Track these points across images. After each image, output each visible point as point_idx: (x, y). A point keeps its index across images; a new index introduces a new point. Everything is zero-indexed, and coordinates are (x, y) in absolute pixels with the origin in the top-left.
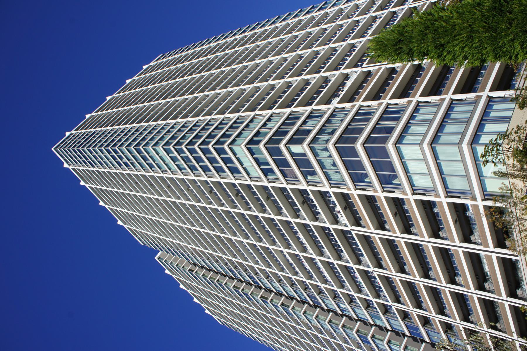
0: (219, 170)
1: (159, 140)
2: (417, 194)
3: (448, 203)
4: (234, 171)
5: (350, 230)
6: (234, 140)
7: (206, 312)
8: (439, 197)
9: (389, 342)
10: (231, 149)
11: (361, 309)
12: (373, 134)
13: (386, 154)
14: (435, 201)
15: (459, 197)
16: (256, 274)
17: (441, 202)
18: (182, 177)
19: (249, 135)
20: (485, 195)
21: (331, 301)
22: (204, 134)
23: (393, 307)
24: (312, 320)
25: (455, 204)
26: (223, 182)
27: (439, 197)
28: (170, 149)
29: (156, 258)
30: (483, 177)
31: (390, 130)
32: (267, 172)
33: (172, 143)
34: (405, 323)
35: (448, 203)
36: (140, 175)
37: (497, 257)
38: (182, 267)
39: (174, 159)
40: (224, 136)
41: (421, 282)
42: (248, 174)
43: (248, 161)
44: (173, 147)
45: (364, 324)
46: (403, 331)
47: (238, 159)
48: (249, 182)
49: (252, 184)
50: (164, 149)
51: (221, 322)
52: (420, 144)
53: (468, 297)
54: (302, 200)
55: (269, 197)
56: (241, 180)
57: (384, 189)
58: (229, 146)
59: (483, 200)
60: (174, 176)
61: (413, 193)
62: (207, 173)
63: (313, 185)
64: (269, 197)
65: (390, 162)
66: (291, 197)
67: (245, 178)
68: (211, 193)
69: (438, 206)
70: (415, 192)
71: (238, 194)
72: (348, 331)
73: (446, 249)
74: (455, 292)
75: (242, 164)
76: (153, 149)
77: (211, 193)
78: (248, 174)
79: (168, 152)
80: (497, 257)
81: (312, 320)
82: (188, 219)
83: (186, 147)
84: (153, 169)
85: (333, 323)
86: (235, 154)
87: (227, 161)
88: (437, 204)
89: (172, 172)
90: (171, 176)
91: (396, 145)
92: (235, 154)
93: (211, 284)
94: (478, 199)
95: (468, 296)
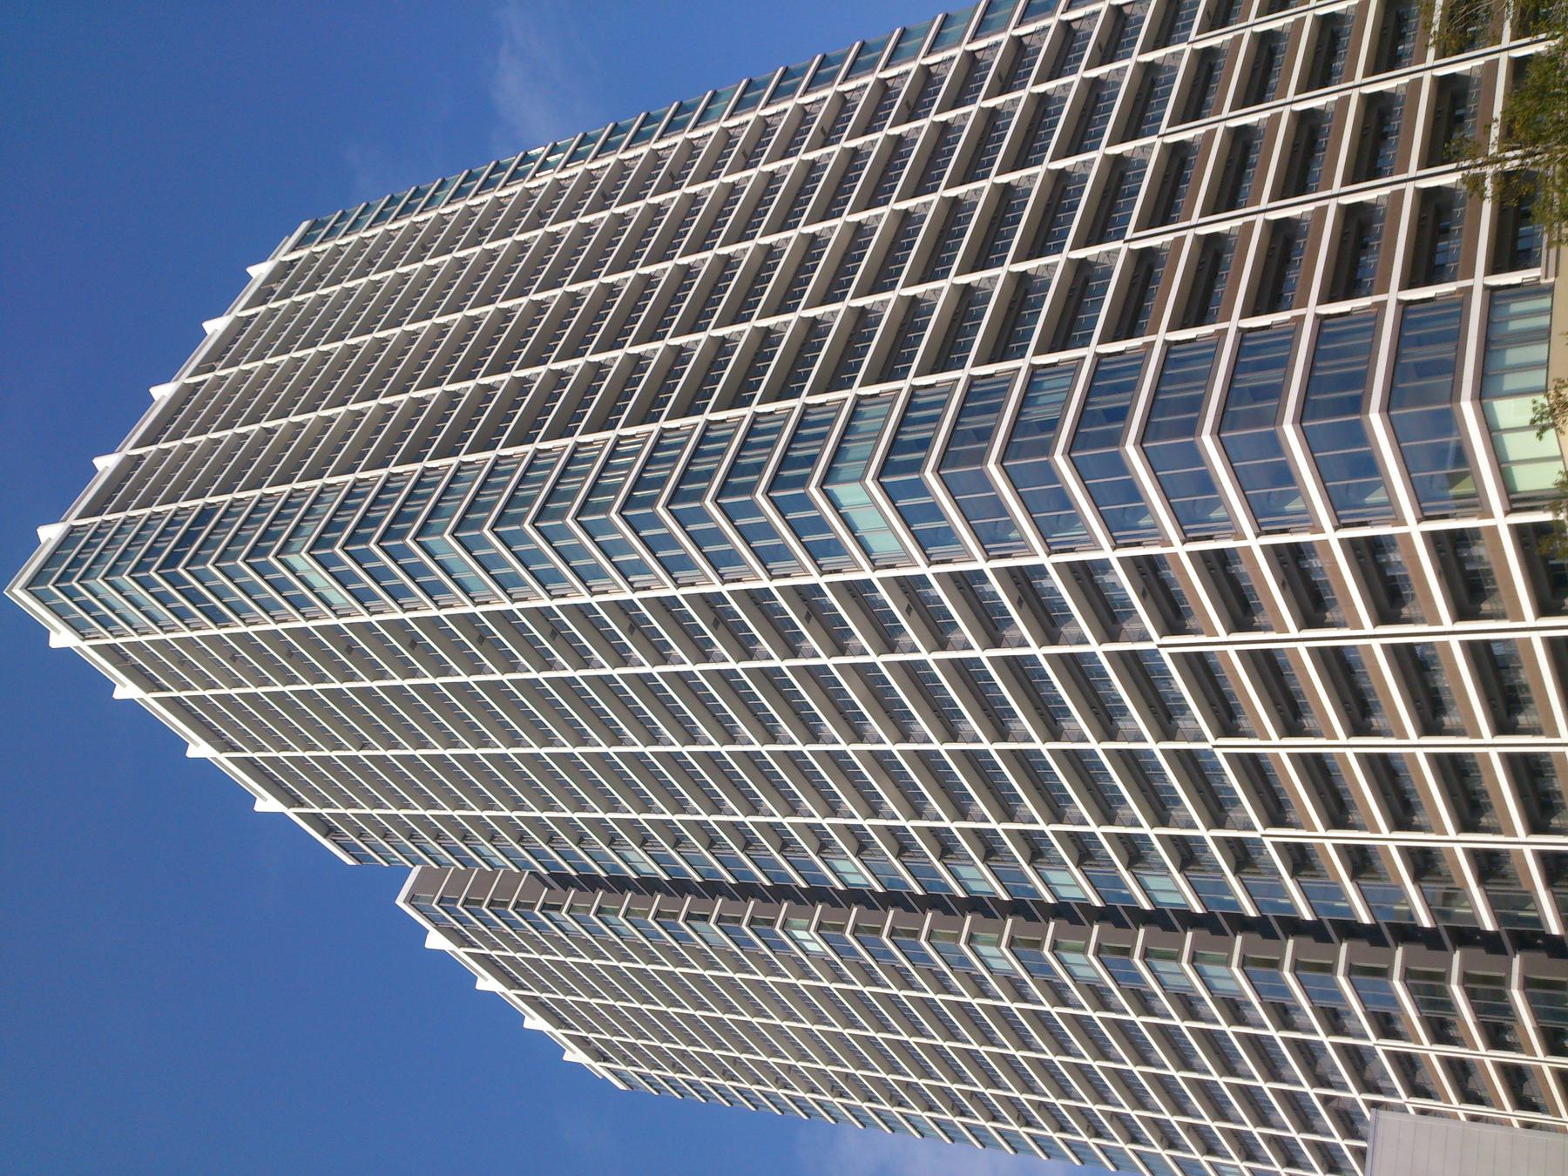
0: (397, 593)
1: (119, 559)
2: (1056, 552)
3: (1190, 554)
4: (298, 603)
5: (1156, 647)
6: (287, 543)
7: (568, 1057)
8: (1170, 544)
9: (971, 939)
10: (421, 545)
11: (848, 859)
12: (685, 484)
13: (811, 505)
14: (1162, 555)
15: (1072, 550)
16: (465, 836)
17: (1326, 543)
18: (187, 634)
19: (314, 530)
20: (1512, 501)
21: (979, 869)
22: (222, 536)
23: (1267, 842)
24: (807, 941)
25: (1134, 559)
26: (445, 616)
27: (1170, 544)
28: (150, 577)
29: (400, 902)
30: (1508, 462)
31: (812, 461)
32: (362, 597)
33: (74, 574)
34: (1083, 871)
35: (1190, 554)
36: (122, 643)
37: (1383, 646)
38: (435, 901)
39: (163, 599)
40: (266, 535)
41: (1279, 748)
42: (328, 605)
43: (321, 578)
44: (377, 543)
45: (731, 900)
46: (869, 886)
47: (301, 579)
48: (333, 621)
49: (341, 622)
50: (313, 557)
51: (624, 1081)
52: (861, 479)
53: (1267, 758)
54: (712, 617)
55: (482, 637)
56: (416, 609)
57: (1118, 542)
58: (495, 530)
59: (1419, 521)
60: (143, 639)
61: (1184, 538)
62: (111, 628)
63: (1001, 557)
64: (482, 637)
65: (934, 504)
66: (647, 619)
67: (426, 605)
68: (554, 639)
69: (1400, 546)
70: (1053, 548)
71: (413, 643)
72: (610, 918)
73: (1200, 654)
74: (1300, 754)
75: (311, 588)
76: (108, 582)
77: (554, 639)
78: (328, 605)
79: (146, 584)
80: (1383, 646)
81: (807, 941)
82: (242, 735)
83: (217, 565)
84: (111, 628)
85: (609, 913)
86: (293, 571)
87: (87, 607)
88: (1168, 561)
89: (135, 630)
90: (136, 638)
91: (1222, 435)
92: (293, 571)
93: (522, 926)
94: (1495, 514)
95: (1269, 756)
